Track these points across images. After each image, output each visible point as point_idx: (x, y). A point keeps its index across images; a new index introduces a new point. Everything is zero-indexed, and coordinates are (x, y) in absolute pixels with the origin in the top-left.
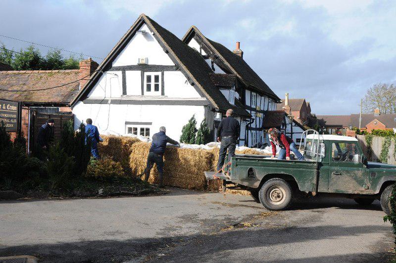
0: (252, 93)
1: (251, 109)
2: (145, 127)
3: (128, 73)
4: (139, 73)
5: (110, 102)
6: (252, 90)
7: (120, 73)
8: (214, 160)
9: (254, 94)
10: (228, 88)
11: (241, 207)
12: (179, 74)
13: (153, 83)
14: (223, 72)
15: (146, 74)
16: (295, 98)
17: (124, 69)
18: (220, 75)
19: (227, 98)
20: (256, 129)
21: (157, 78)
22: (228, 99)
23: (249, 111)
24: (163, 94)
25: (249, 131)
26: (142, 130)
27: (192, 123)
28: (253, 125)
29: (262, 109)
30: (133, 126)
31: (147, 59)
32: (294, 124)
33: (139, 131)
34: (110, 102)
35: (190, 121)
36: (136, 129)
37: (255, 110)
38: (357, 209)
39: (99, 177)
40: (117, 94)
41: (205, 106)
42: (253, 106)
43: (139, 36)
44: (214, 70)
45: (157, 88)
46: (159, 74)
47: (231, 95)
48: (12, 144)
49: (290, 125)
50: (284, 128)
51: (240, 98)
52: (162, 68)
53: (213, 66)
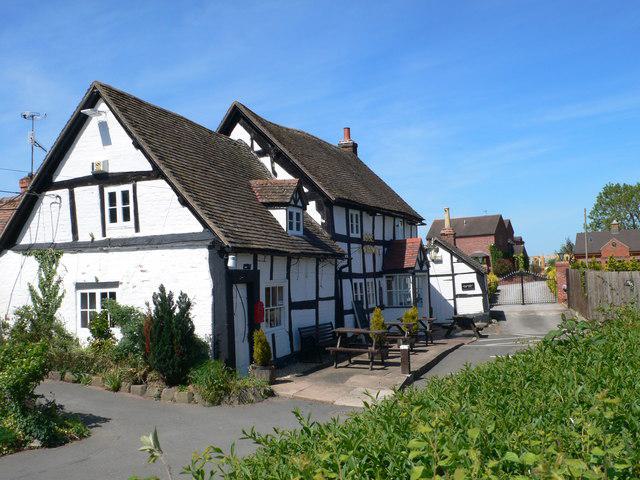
0: (351, 211)
2: (108, 291)
3: (77, 190)
4: (95, 188)
9: (354, 212)
13: (119, 206)
15: (108, 190)
16: (455, 217)
17: (71, 184)
21: (125, 194)
24: (137, 229)
26: (104, 295)
29: (379, 236)
31: (106, 163)
32: (455, 259)
36: (93, 296)
41: (210, 248)
44: (275, 174)
45: (126, 217)
46: (128, 187)
48: (205, 345)
50: (425, 268)
53: (273, 168)
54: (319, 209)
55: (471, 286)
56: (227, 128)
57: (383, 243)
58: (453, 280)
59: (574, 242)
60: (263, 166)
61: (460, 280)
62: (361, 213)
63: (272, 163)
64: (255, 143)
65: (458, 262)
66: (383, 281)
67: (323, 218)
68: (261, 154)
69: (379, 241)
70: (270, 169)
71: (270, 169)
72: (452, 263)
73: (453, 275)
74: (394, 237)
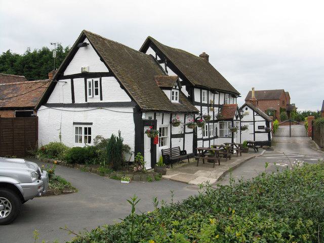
1: (201, 104)
2: (88, 126)
7: (69, 81)
11: (176, 179)
15: (89, 80)
17: (72, 77)
21: (96, 82)
32: (255, 114)
36: (81, 128)
38: (144, 149)
42: (206, 102)
44: (167, 72)
46: (98, 79)
48: (127, 148)
52: (101, 75)
53: (166, 69)
54: (187, 89)
56: (144, 49)
58: (254, 124)
61: (257, 124)
63: (166, 66)
64: (158, 56)
68: (161, 62)
72: (254, 115)
73: (254, 122)
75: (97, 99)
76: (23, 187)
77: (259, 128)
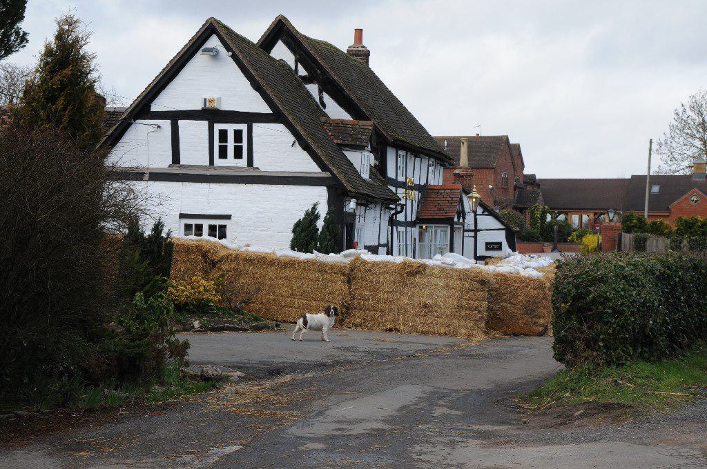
1: (399, 185)
2: (217, 223)
4: (204, 124)
5: (147, 176)
6: (399, 145)
7: (166, 124)
8: (268, 362)
9: (401, 153)
10: (360, 148)
12: (279, 129)
14: (345, 116)
15: (218, 127)
17: (175, 117)
18: (342, 122)
19: (357, 166)
20: (407, 224)
21: (238, 135)
22: (359, 171)
23: (393, 189)
25: (394, 228)
27: (312, 216)
28: (400, 217)
29: (416, 182)
30: (193, 222)
32: (480, 210)
33: (206, 230)
34: (147, 176)
35: (307, 214)
37: (403, 185)
39: (186, 304)
40: (162, 161)
41: (329, 188)
42: (402, 179)
43: (199, 59)
44: (324, 106)
45: (238, 154)
46: (243, 127)
47: (362, 161)
49: (473, 215)
50: (461, 220)
51: (377, 163)
52: (250, 118)
53: (321, 98)
55: (498, 246)
56: (268, 42)
57: (419, 188)
58: (475, 237)
59: (54, 46)
60: (310, 96)
61: (483, 238)
62: (407, 154)
63: (320, 92)
64: (300, 66)
65: (483, 214)
66: (415, 231)
67: (376, 159)
68: (307, 80)
69: (401, 187)
70: (317, 100)
71: (317, 100)
73: (476, 231)
74: (427, 183)
75: (231, 162)
76: (470, 259)
77: (487, 249)
